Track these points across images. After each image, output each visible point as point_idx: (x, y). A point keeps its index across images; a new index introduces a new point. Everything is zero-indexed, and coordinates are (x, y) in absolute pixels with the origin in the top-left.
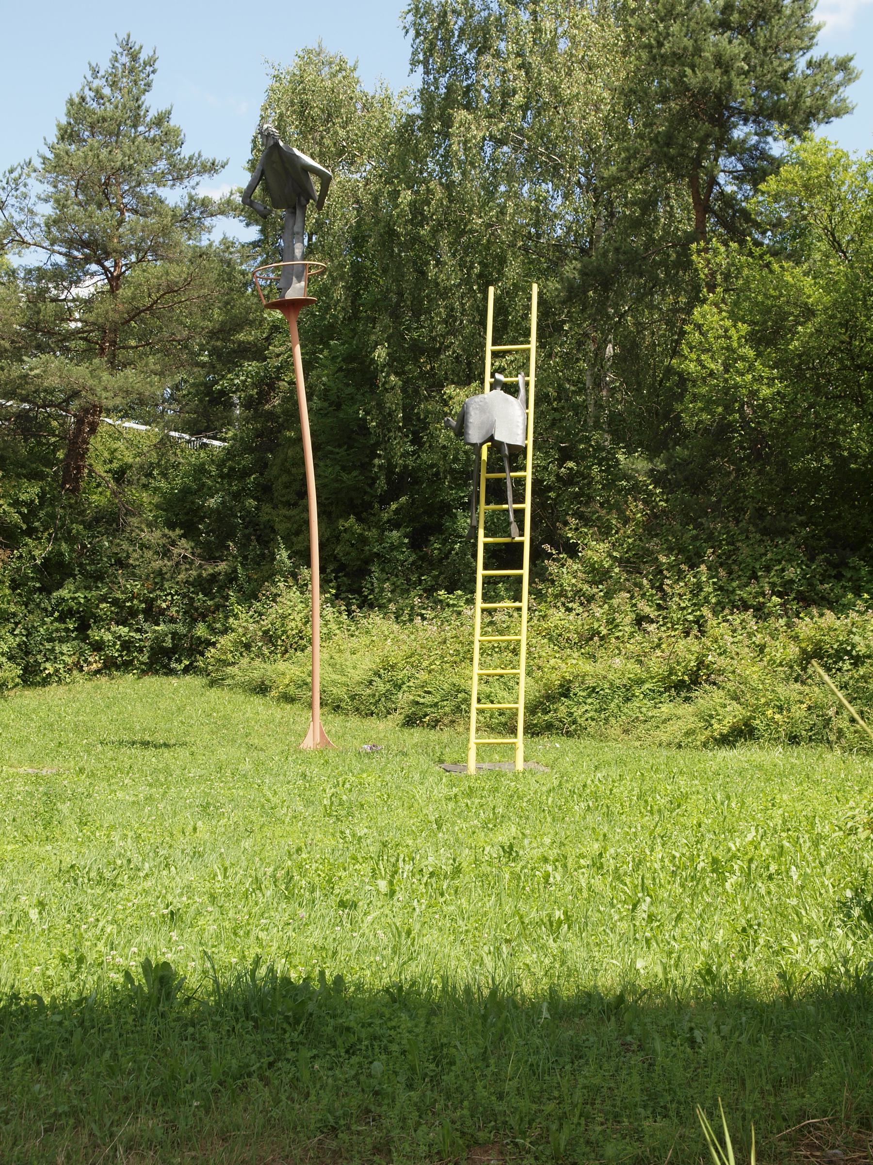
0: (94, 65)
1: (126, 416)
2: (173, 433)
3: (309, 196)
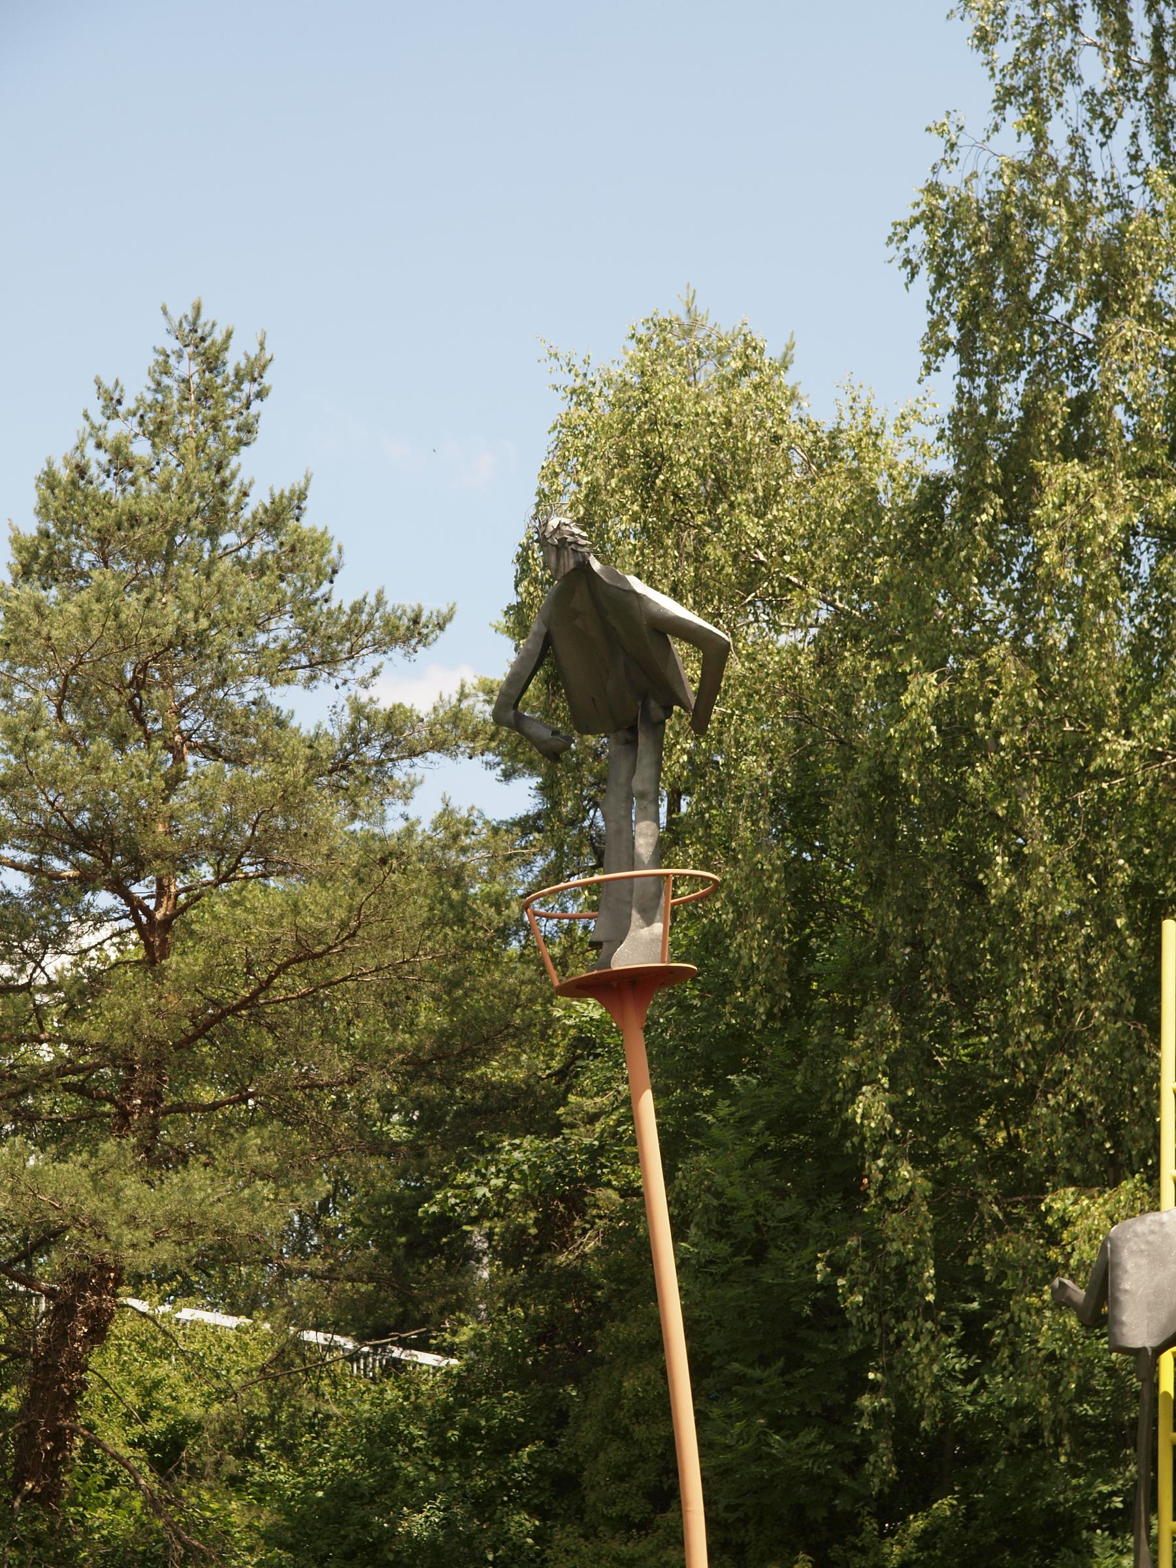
0: (109, 384)
2: (310, 1336)
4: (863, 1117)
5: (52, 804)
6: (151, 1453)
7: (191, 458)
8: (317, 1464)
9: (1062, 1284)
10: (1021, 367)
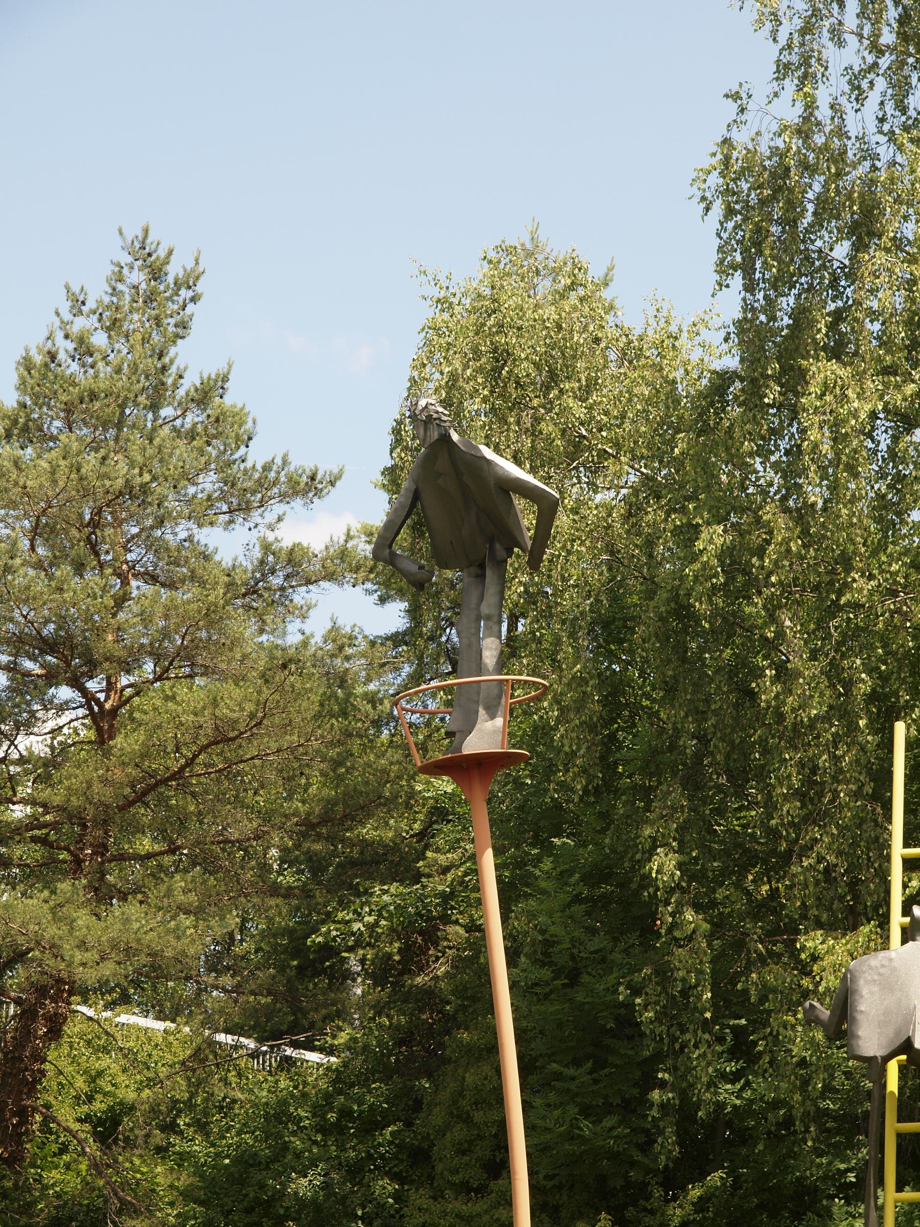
0: (76, 289)
2: (221, 1037)
3: (511, 540)
4: (657, 872)
5: (25, 617)
6: (95, 1127)
7: (138, 347)
8: (225, 1138)
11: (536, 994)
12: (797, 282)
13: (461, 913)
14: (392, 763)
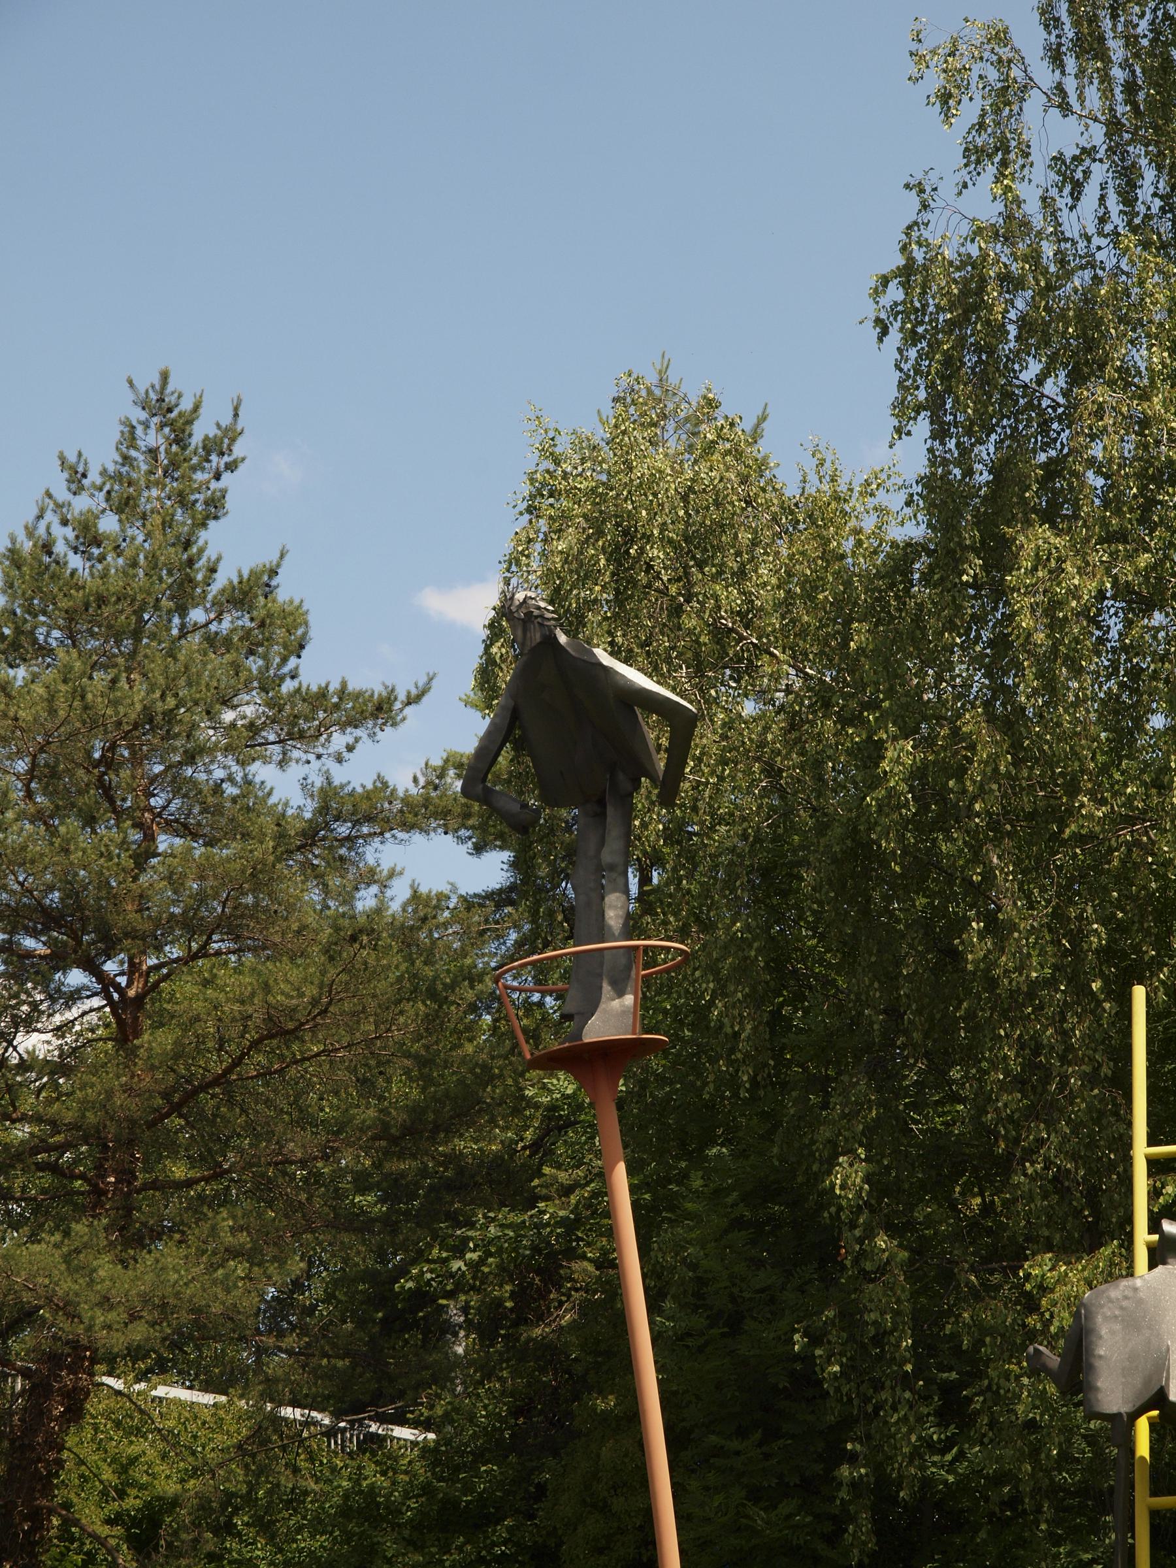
0: (72, 458)
1: (161, 1369)
2: (288, 1412)
3: (639, 767)
4: (842, 1187)
5: (21, 884)
6: (128, 1530)
7: (158, 534)
8: (295, 1541)
9: (1036, 1350)
10: (992, 430)
11: (688, 1347)
12: (997, 425)
13: (589, 1245)
14: (493, 1058)
